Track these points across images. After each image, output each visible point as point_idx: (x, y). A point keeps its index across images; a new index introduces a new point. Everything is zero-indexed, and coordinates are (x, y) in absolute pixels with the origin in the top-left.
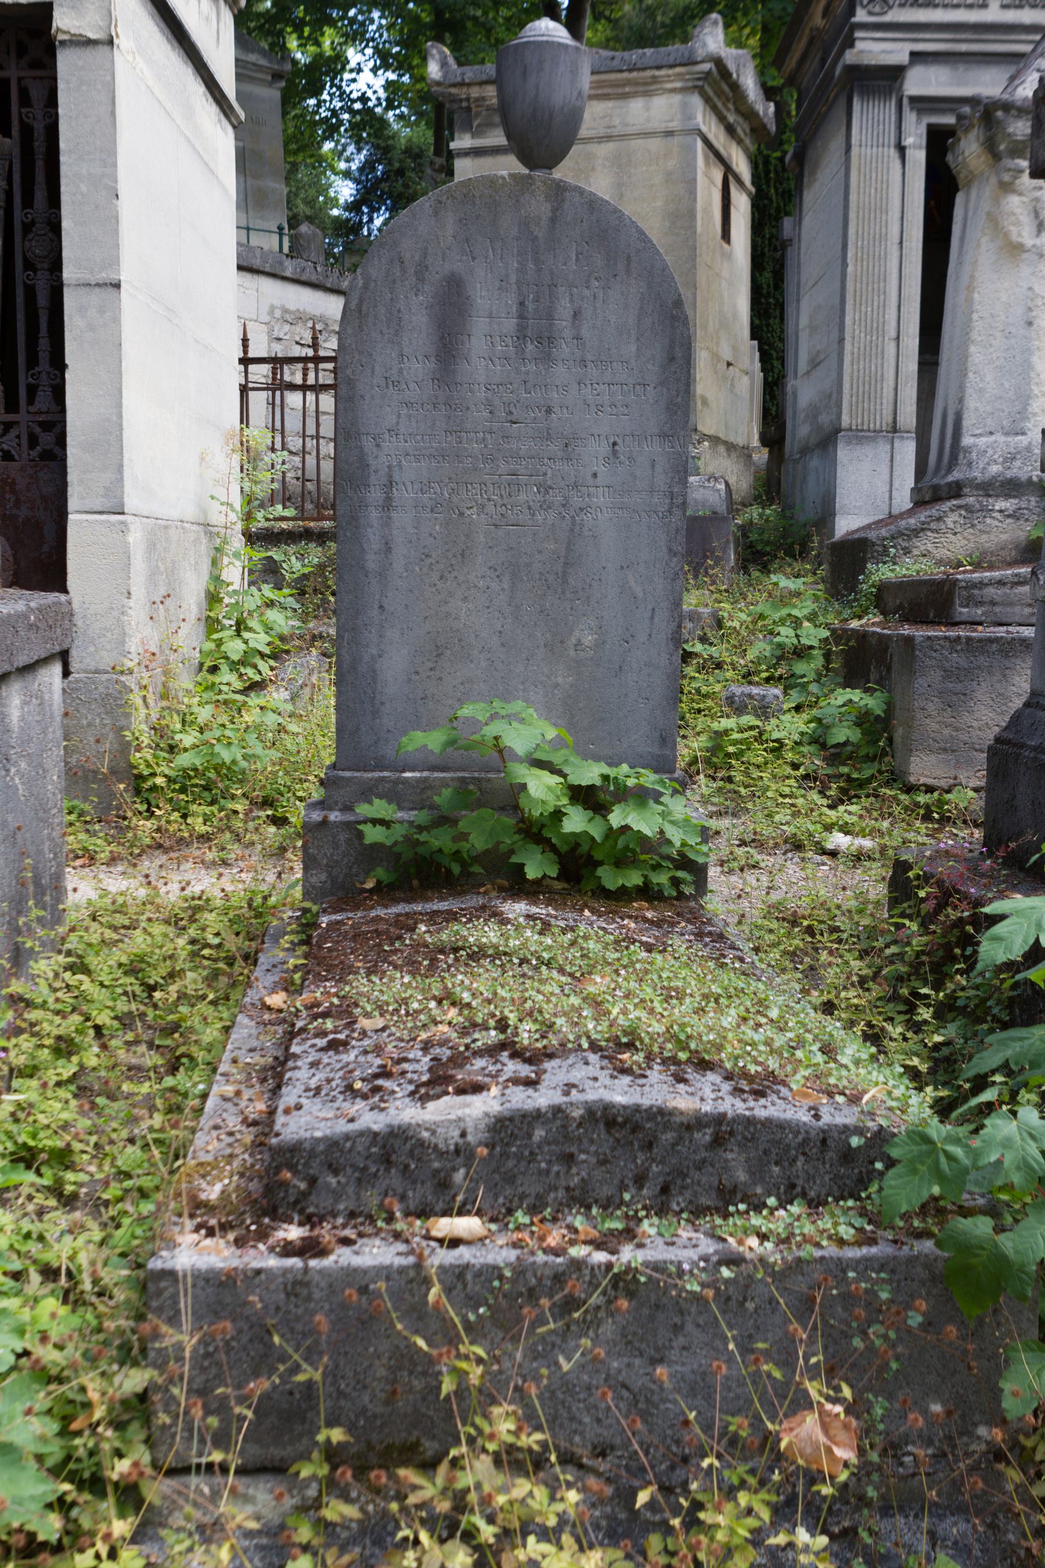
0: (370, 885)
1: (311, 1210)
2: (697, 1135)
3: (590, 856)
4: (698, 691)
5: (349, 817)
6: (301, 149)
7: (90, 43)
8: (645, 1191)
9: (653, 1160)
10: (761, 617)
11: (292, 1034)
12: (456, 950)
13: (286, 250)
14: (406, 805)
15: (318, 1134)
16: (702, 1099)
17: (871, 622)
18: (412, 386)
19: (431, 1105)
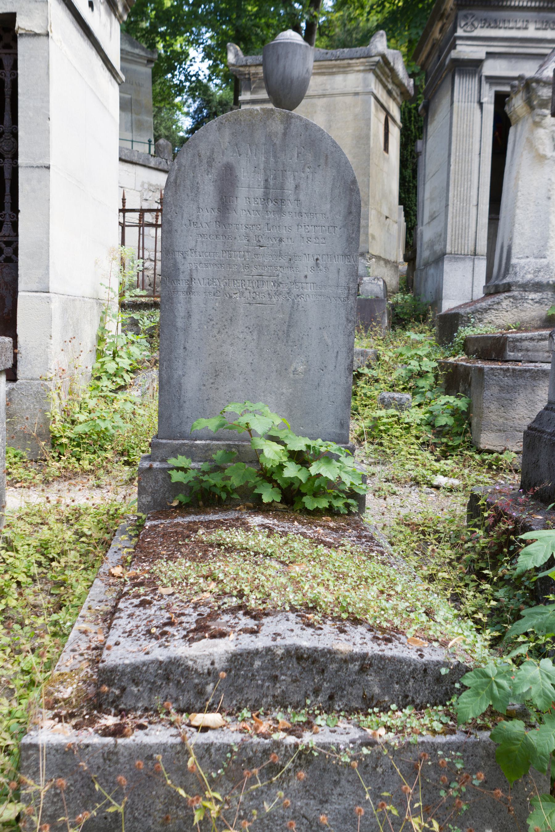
0: (175, 504)
1: (122, 706)
2: (351, 666)
3: (299, 491)
4: (365, 394)
5: (164, 466)
6: (163, 100)
7: (36, 35)
8: (319, 698)
9: (325, 680)
10: (401, 354)
11: (121, 595)
12: (219, 545)
13: (152, 152)
14: (197, 459)
15: (127, 662)
16: (354, 644)
17: (461, 359)
18: (204, 225)
19: (195, 645)
